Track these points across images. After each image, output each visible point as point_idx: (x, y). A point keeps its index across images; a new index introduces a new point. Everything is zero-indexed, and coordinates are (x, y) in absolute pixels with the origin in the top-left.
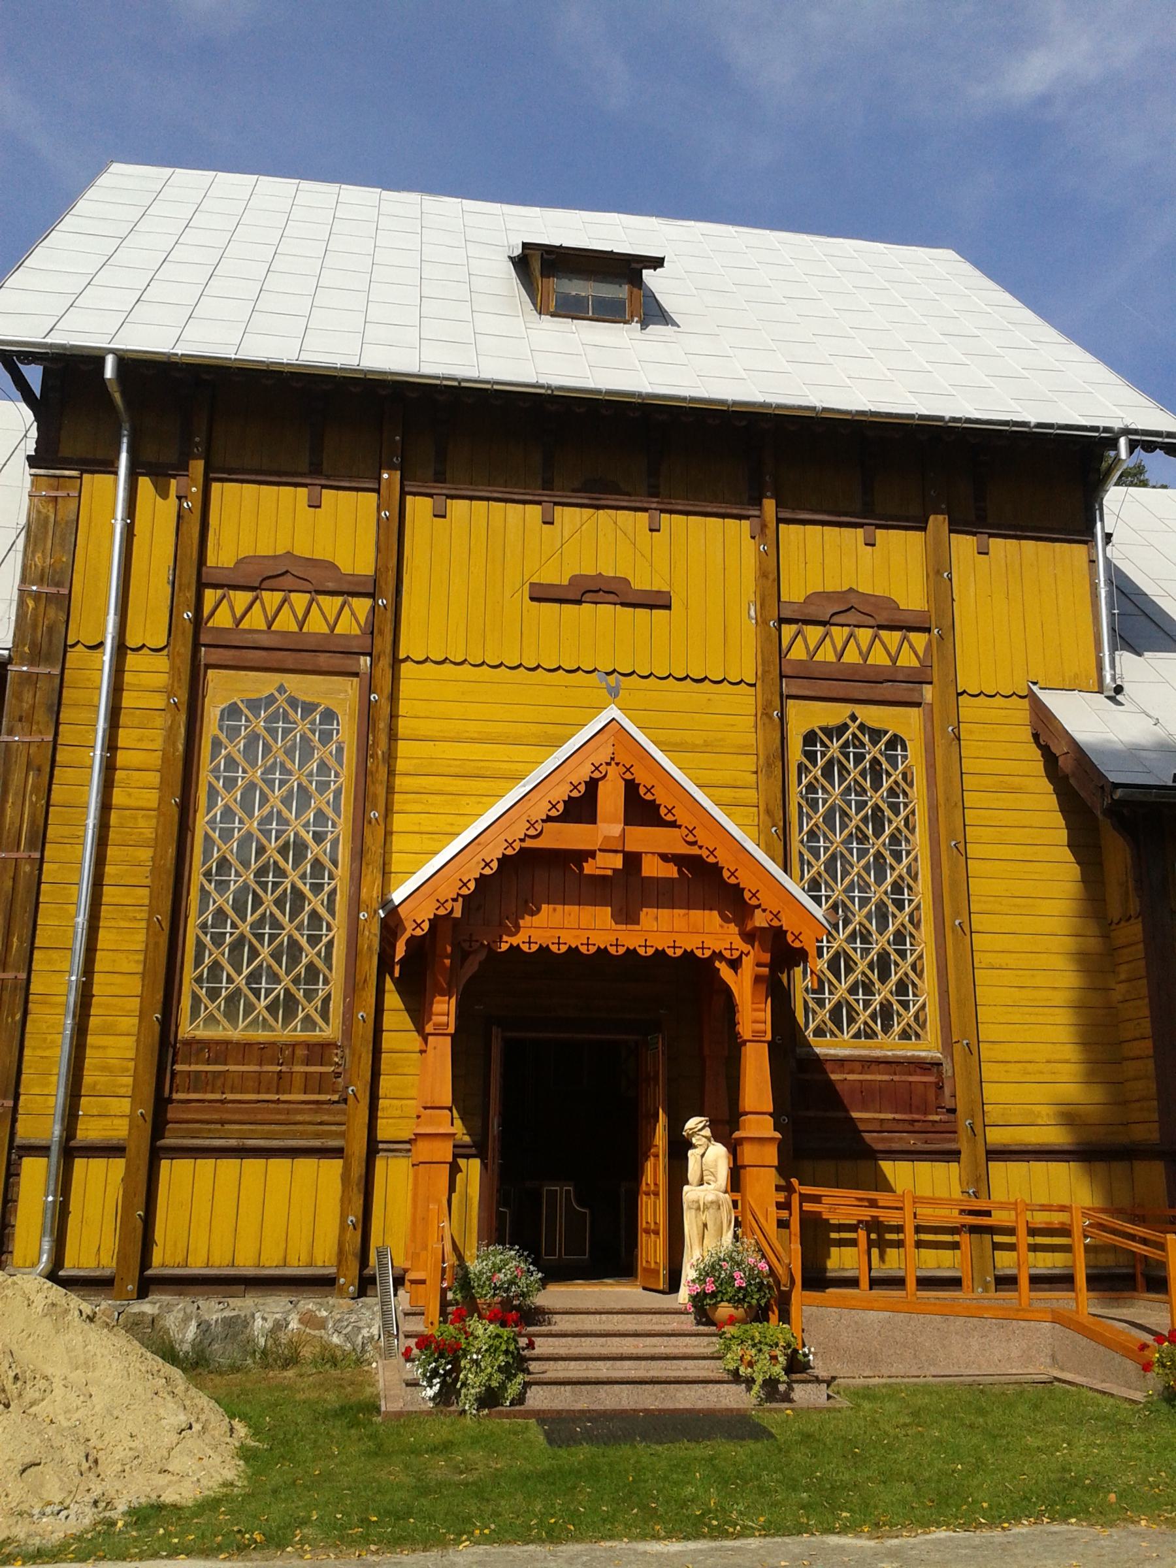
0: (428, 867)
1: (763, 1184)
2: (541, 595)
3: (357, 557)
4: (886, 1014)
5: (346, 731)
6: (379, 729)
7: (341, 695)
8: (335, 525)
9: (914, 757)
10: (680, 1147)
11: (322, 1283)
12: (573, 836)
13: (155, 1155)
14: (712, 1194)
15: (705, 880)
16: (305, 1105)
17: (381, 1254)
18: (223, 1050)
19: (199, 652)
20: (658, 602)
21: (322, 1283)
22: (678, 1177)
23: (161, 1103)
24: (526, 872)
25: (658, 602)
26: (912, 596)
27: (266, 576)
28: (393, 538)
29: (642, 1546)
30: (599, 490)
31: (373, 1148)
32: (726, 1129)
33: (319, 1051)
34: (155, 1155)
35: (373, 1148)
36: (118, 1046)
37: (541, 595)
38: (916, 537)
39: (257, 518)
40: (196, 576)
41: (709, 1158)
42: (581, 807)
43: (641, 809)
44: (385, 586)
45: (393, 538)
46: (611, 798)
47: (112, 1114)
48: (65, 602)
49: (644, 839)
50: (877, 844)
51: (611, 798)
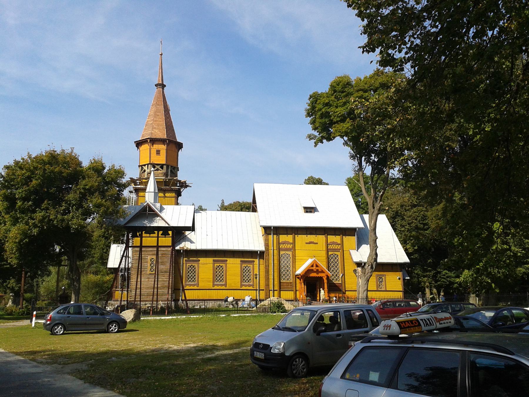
0: (300, 271)
1: (327, 293)
2: (306, 243)
3: (291, 241)
4: (337, 279)
5: (291, 256)
6: (294, 256)
7: (290, 253)
8: (289, 238)
9: (339, 256)
10: (320, 291)
11: (293, 300)
12: (312, 268)
13: (280, 291)
14: (323, 294)
15: (323, 272)
16: (291, 287)
17: (382, 334)
18: (284, 283)
19: (279, 250)
20: (317, 243)
21: (293, 300)
22: (320, 293)
23: (280, 287)
24: (308, 271)
25: (317, 243)
26: (339, 242)
27: (284, 243)
28: (294, 239)
29: (195, 345)
30: (311, 234)
31: (296, 291)
32: (323, 289)
33: (291, 283)
34: (280, 291)
35: (296, 291)
36: (276, 282)
37: (306, 243)
38: (339, 237)
39: (283, 238)
40: (279, 243)
41: (322, 292)
42: (312, 266)
43: (317, 266)
44: (294, 243)
45: (294, 239)
46: (315, 265)
47: (276, 288)
48: (268, 246)
49: (317, 268)
50: (336, 260)
51: (315, 265)
